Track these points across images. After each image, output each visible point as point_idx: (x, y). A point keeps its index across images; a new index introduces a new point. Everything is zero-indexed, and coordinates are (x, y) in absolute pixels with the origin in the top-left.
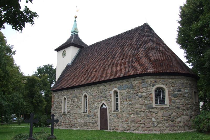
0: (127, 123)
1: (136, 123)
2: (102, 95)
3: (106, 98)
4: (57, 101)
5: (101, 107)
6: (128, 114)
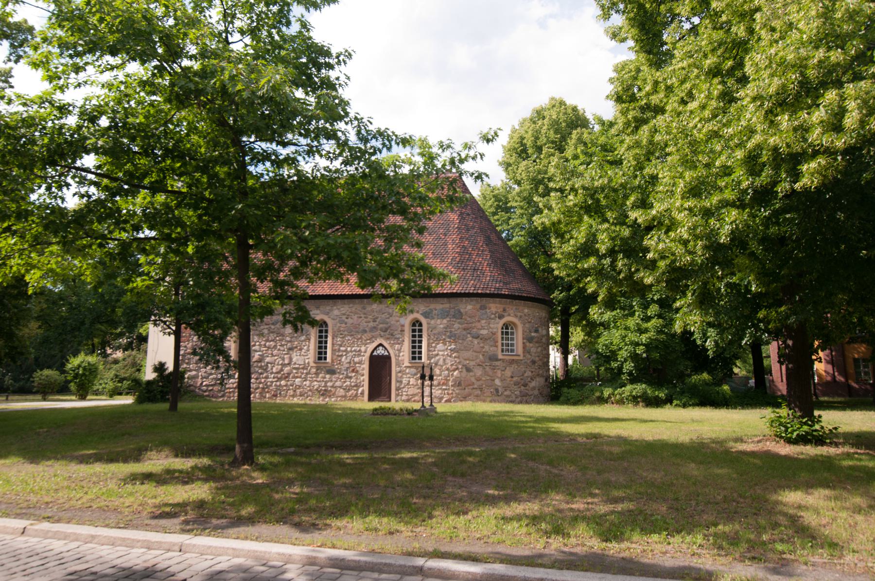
3: (389, 332)
5: (373, 352)
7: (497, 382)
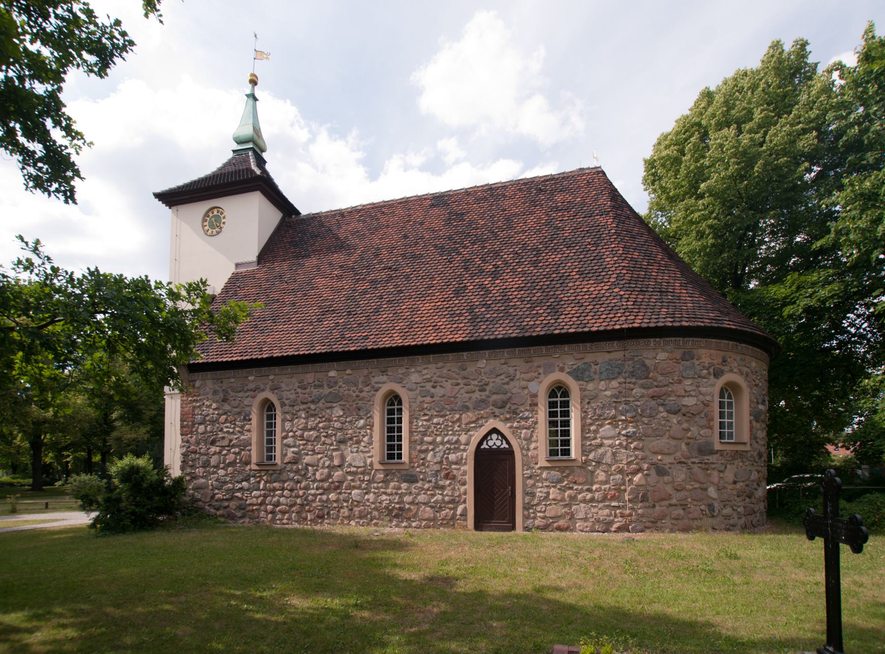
2: (483, 397)
5: (481, 443)
7: (712, 492)
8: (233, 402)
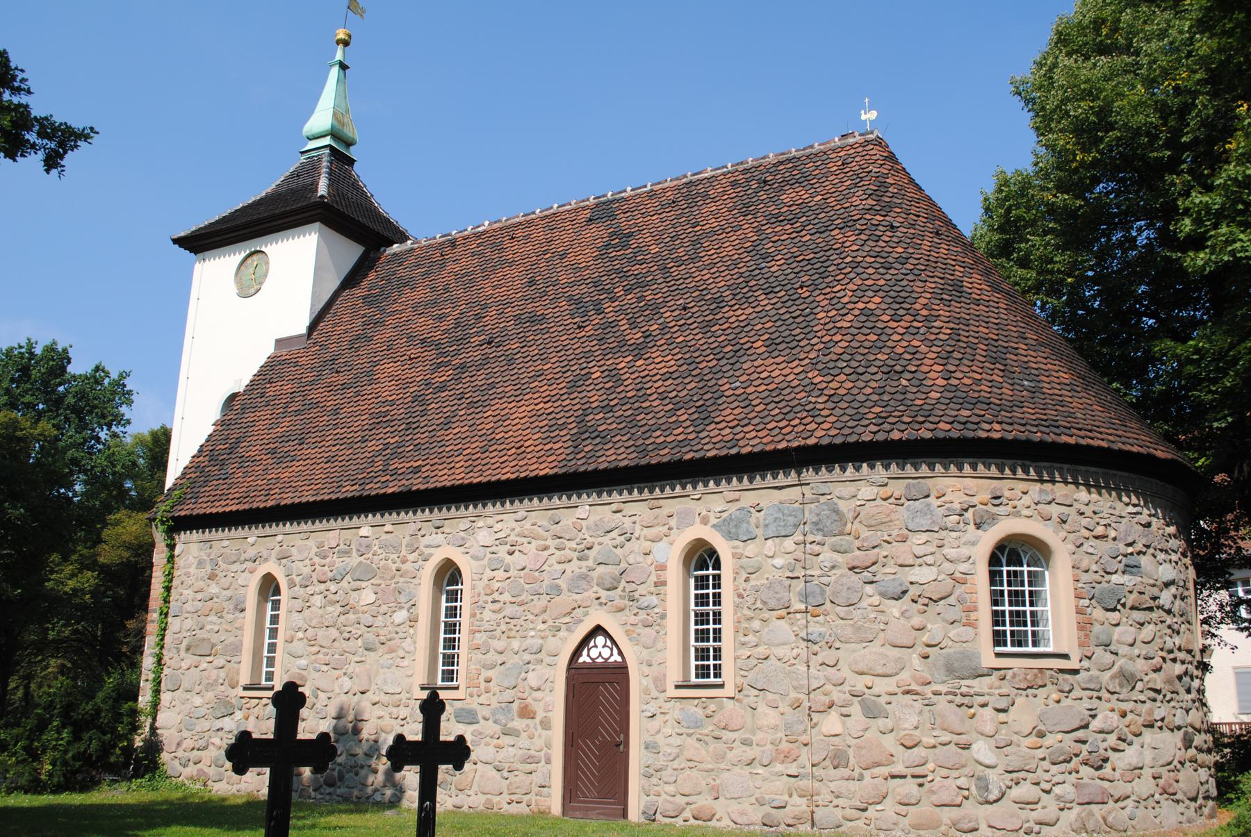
0: (793, 772)
1: (856, 774)
2: (584, 570)
4: (199, 596)
6: (797, 706)
7: (982, 750)
8: (224, 580)
